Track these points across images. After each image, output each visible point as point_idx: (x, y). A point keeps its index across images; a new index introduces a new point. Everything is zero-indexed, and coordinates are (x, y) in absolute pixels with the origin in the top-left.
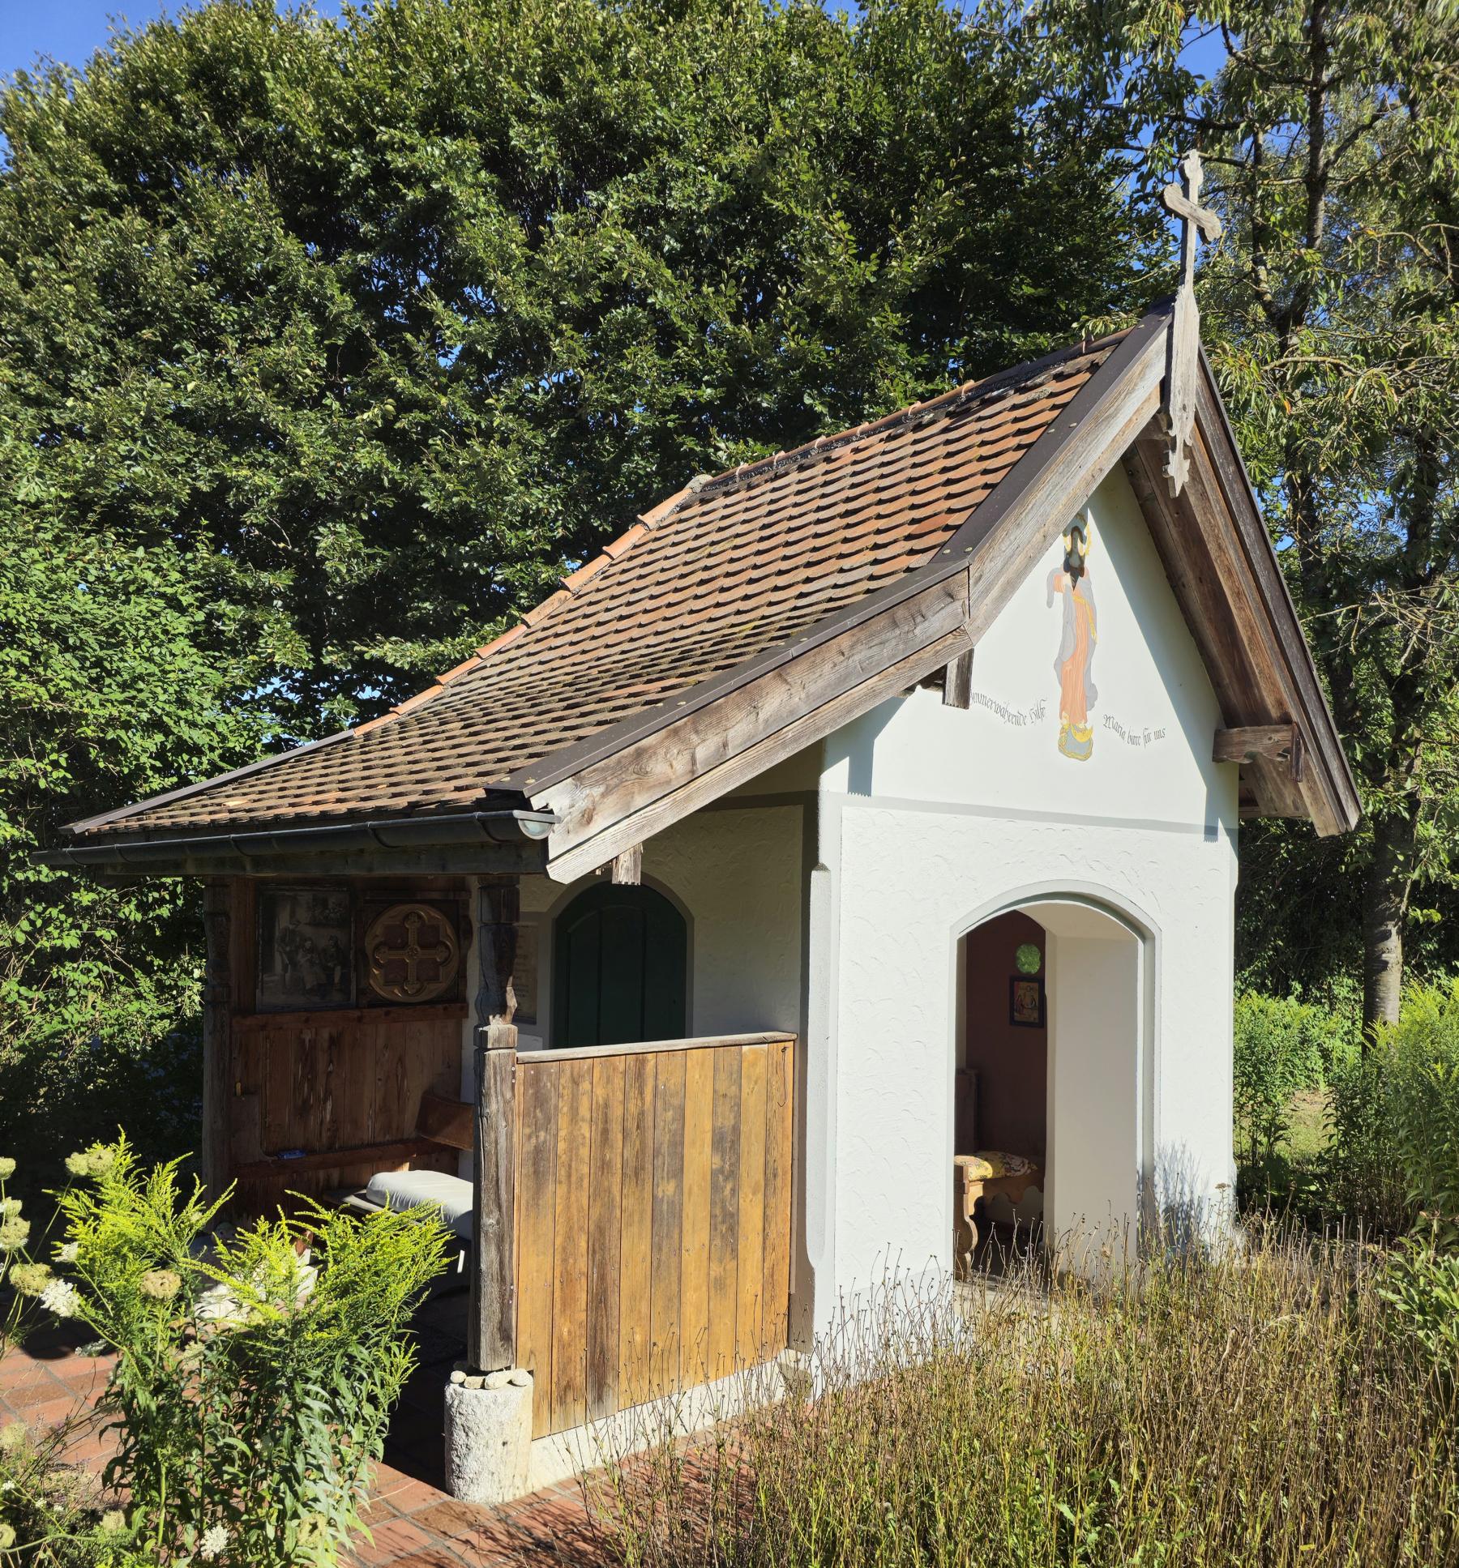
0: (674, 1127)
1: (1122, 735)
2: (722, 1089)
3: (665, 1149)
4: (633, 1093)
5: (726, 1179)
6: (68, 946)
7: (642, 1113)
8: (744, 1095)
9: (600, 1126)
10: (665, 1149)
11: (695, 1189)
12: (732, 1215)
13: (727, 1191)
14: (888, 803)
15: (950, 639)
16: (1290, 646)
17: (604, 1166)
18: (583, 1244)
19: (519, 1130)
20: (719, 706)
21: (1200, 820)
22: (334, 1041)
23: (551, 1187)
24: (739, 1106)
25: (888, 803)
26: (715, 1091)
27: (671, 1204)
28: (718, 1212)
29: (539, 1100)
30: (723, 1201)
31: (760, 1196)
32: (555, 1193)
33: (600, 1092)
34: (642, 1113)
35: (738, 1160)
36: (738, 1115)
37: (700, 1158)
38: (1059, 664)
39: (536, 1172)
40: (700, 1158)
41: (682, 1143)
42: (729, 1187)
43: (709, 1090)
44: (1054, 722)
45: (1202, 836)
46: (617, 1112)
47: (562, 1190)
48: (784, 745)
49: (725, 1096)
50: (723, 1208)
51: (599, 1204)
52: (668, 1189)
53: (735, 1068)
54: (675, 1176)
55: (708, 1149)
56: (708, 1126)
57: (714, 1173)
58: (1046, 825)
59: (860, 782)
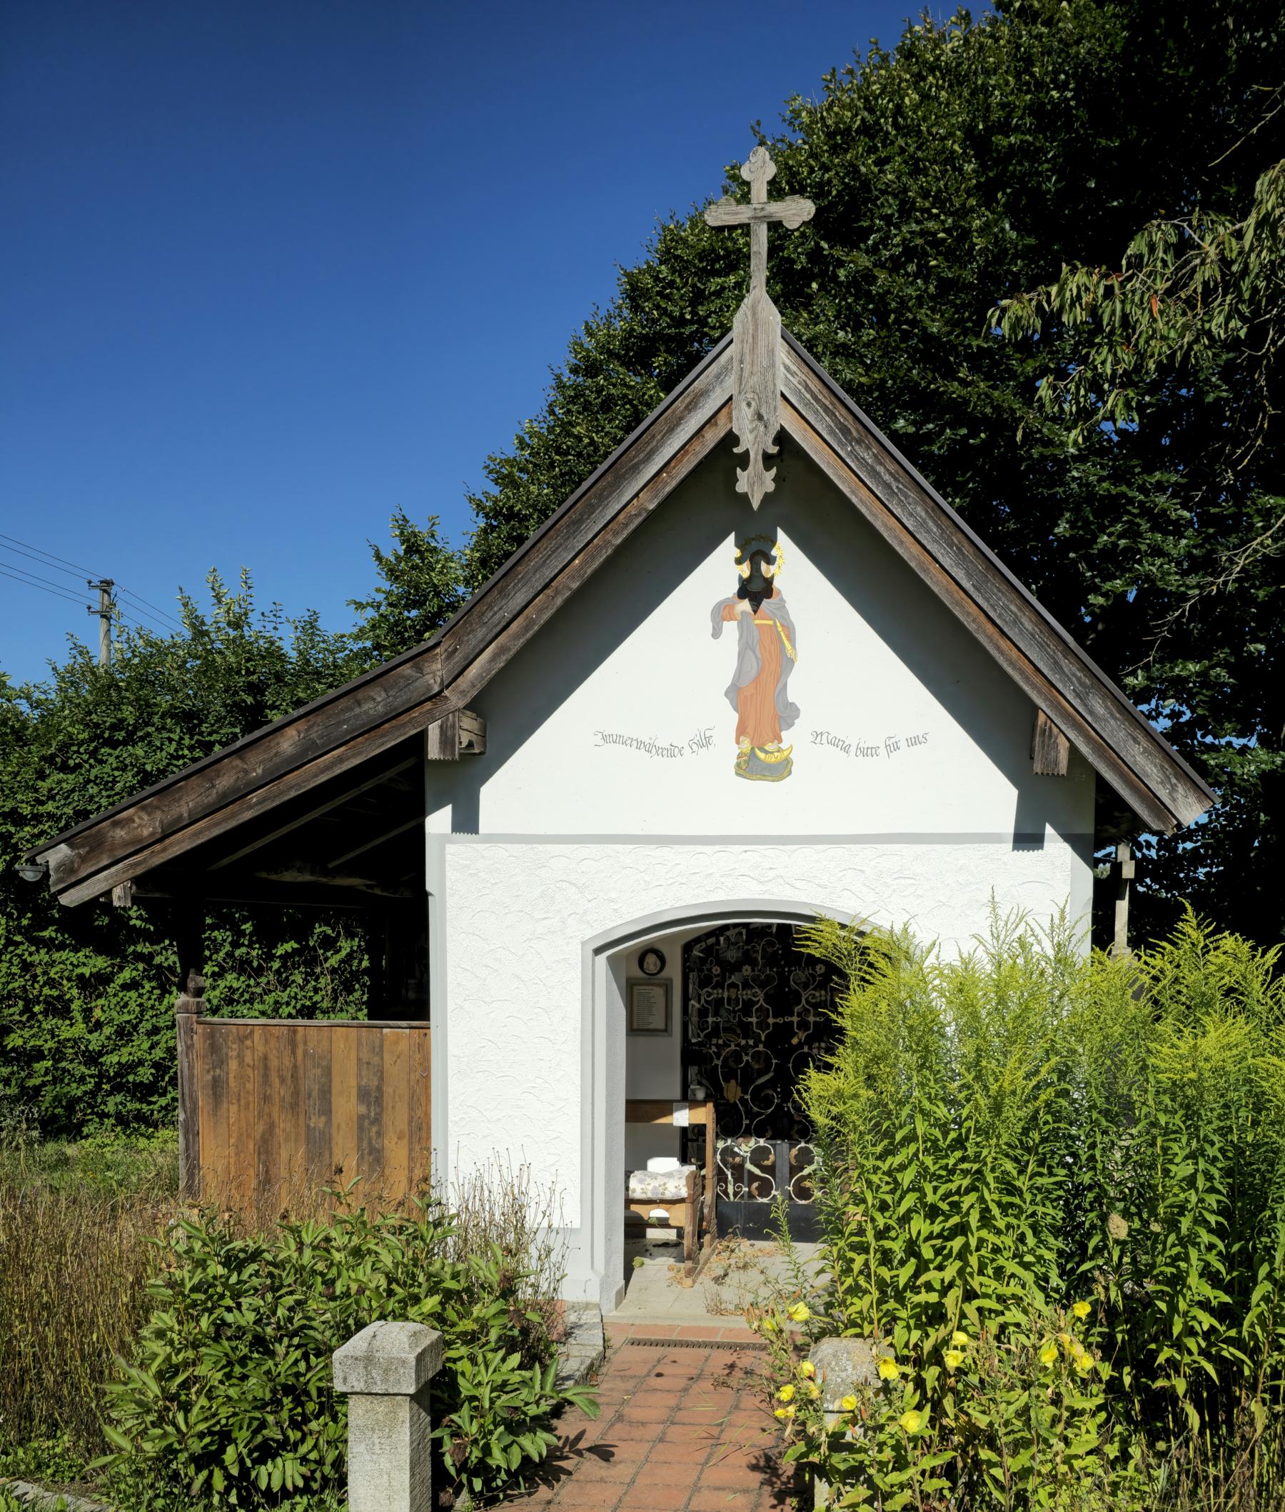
0: (323, 1080)
1: (846, 749)
2: (365, 1056)
3: (315, 1094)
4: (287, 1052)
5: (372, 1123)
6: (290, 950)
7: (295, 1066)
8: (387, 1065)
9: (262, 1072)
10: (315, 1094)
11: (343, 1126)
12: (378, 1151)
13: (373, 1134)
14: (493, 839)
15: (428, 706)
16: (1016, 622)
17: (266, 1099)
18: (251, 1146)
19: (199, 1067)
20: (181, 788)
21: (1008, 825)
22: (1206, 1060)
23: (225, 1105)
24: (382, 1072)
25: (493, 839)
26: (359, 1059)
27: (322, 1133)
28: (365, 1145)
29: (214, 1048)
30: (370, 1139)
31: (406, 1141)
32: (232, 1110)
33: (260, 1049)
34: (295, 1066)
35: (382, 1111)
36: (381, 1079)
37: (346, 1106)
38: (736, 693)
39: (215, 1094)
40: (346, 1106)
41: (330, 1092)
42: (374, 1129)
43: (353, 1056)
44: (728, 749)
45: (1010, 845)
46: (274, 1063)
47: (234, 1109)
48: (250, 808)
49: (368, 1063)
50: (370, 1143)
51: (262, 1122)
52: (318, 1122)
53: (378, 1044)
54: (324, 1114)
55: (354, 1099)
56: (353, 1082)
57: (361, 1118)
58: (717, 848)
59: (466, 822)
